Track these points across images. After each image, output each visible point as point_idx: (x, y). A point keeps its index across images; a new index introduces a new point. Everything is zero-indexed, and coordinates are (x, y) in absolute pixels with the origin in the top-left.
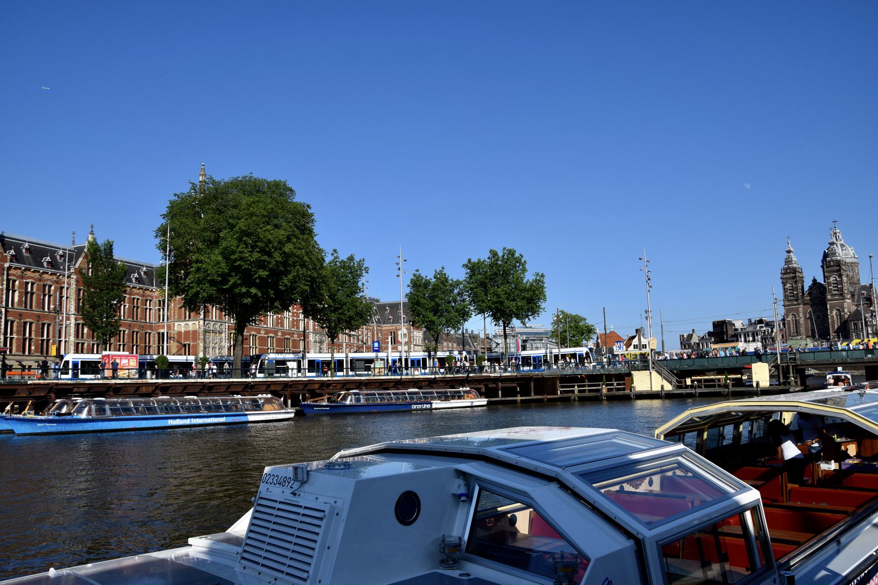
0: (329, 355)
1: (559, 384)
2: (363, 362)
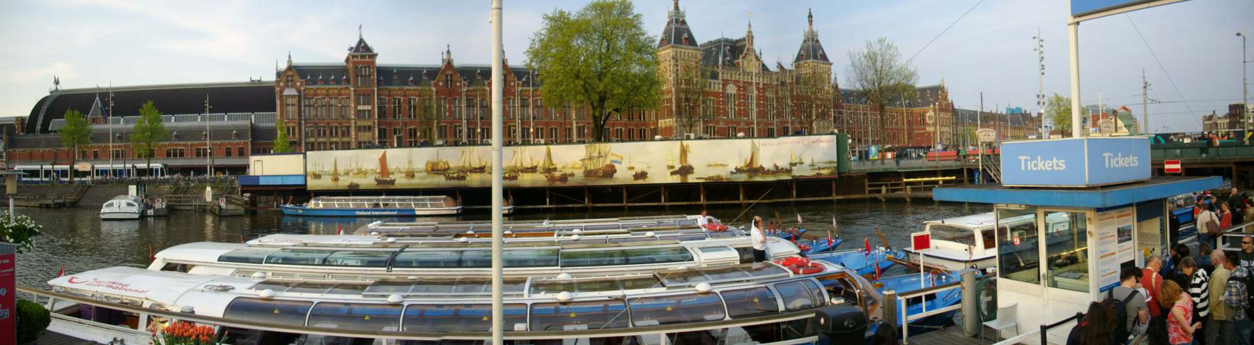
0: (123, 166)
1: (867, 183)
2: (1198, 150)
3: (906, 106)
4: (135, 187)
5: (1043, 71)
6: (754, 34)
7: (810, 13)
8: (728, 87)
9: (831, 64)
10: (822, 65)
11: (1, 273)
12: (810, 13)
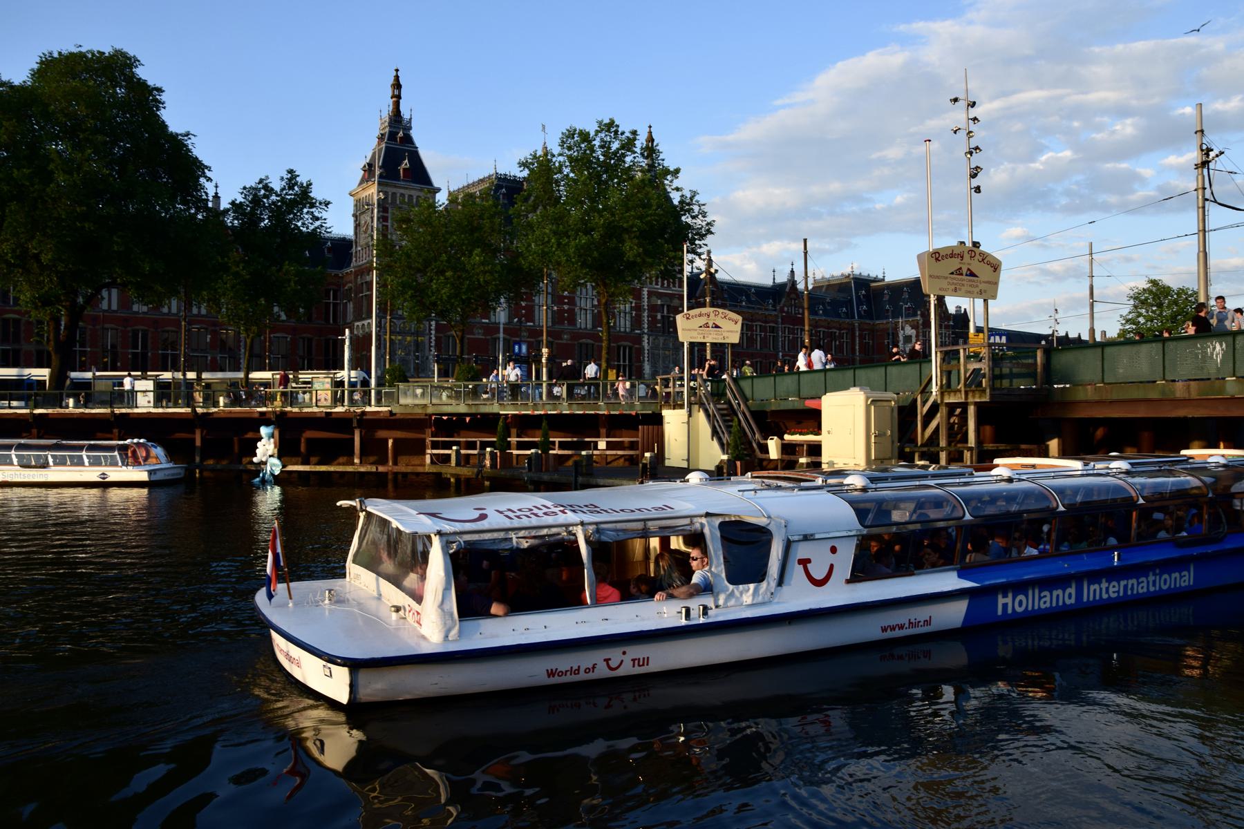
3: (860, 316)
4: (195, 377)
5: (975, 182)
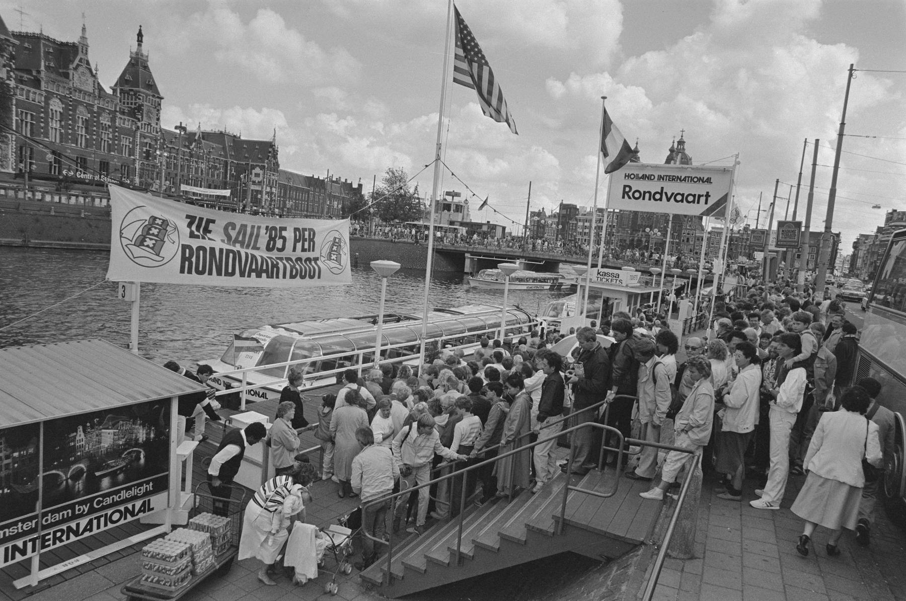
6: (89, 42)
7: (140, 30)
8: (51, 102)
9: (162, 98)
10: (151, 97)
11: (905, 227)
12: (140, 30)
